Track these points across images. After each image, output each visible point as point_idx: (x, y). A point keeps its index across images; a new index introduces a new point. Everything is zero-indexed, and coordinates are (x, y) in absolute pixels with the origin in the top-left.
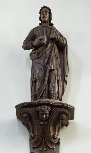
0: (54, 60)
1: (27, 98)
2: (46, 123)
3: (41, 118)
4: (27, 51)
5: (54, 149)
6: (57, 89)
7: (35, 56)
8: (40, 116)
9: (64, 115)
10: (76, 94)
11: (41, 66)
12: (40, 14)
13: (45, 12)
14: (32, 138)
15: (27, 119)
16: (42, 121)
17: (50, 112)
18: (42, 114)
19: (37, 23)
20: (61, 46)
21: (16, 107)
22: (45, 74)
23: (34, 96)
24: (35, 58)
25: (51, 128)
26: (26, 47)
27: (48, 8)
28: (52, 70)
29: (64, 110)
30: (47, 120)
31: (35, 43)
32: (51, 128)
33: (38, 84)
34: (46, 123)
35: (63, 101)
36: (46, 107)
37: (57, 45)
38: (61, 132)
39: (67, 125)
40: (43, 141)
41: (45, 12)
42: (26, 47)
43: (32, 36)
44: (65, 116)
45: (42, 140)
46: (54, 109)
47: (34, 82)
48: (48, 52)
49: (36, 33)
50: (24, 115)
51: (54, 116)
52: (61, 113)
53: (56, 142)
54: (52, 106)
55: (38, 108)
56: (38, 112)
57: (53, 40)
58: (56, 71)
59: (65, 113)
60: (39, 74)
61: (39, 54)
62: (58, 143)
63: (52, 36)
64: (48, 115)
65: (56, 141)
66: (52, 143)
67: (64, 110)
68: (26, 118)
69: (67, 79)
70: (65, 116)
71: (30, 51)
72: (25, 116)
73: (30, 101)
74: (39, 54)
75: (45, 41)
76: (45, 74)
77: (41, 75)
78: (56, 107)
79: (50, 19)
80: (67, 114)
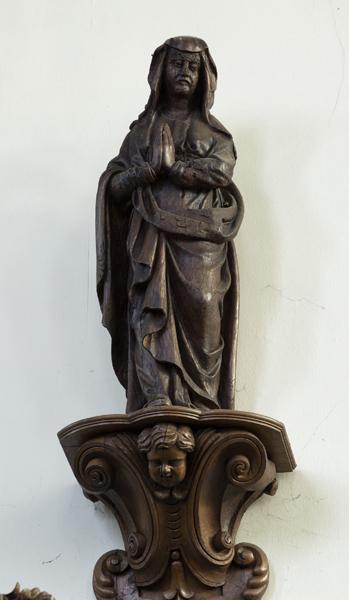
2: (178, 496)
3: (155, 475)
4: (160, 42)
5: (221, 587)
9: (253, 455)
10: (279, 373)
12: (137, 118)
15: (104, 481)
16: (161, 488)
18: (159, 462)
21: (61, 435)
25: (203, 512)
30: (187, 484)
32: (203, 512)
34: (178, 496)
39: (270, 489)
40: (175, 563)
44: (248, 462)
45: (171, 561)
50: (94, 463)
51: (209, 468)
64: (182, 466)
65: (228, 556)
68: (101, 475)
70: (246, 460)
72: (99, 468)
73: (124, 413)
78: (211, 432)
80: (243, 443)
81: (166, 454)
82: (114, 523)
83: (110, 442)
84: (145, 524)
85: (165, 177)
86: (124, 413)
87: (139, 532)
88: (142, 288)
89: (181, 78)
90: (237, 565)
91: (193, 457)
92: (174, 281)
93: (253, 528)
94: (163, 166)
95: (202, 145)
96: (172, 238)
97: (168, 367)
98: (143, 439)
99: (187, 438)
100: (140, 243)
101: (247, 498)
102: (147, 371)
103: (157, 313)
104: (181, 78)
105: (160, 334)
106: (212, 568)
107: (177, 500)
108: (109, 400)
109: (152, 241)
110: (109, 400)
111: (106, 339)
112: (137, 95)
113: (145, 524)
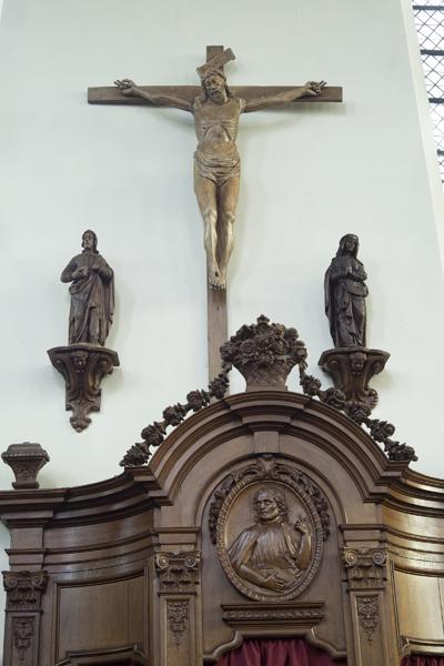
0: (97, 295)
1: (64, 342)
6: (98, 330)
7: (74, 291)
11: (431, 22)
13: (90, 238)
14: (68, 388)
16: (77, 369)
19: (79, 250)
20: (106, 278)
21: (48, 352)
23: (73, 339)
24: (74, 291)
26: (65, 280)
27: (92, 233)
28: (92, 308)
29: (103, 356)
30: (84, 368)
31: (74, 274)
33: (76, 324)
35: (106, 346)
36: (82, 352)
37: (314, 96)
39: (110, 373)
41: (90, 238)
42: (65, 280)
43: (72, 267)
46: (92, 355)
47: (72, 323)
48: (89, 286)
49: (77, 262)
51: (93, 364)
52: (100, 360)
53: (96, 392)
54: (90, 351)
55: (73, 354)
56: (72, 358)
57: (96, 271)
59: (105, 360)
60: (78, 312)
61: (78, 288)
62: (99, 395)
63: (95, 267)
66: (92, 395)
67: (103, 356)
69: (114, 318)
71: (70, 284)
74: (78, 288)
75: (85, 273)
76: (85, 312)
79: (95, 246)
83: (340, 356)
84: (346, 381)
85: (349, 276)
88: (344, 310)
89: (349, 246)
91: (366, 363)
93: (374, 384)
94: (349, 274)
95: (357, 267)
97: (352, 334)
98: (352, 356)
101: (103, 376)
102: (345, 334)
104: (349, 246)
107: (81, 377)
112: (335, 247)
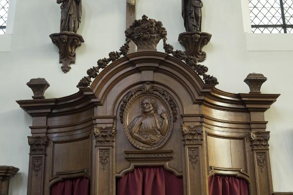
0: (72, 9)
1: (57, 30)
6: (73, 26)
8: (194, 40)
17: (67, 39)
22: (67, 18)
23: (62, 29)
29: (76, 38)
30: (66, 43)
32: (199, 47)
36: (65, 36)
38: (77, 49)
39: (80, 45)
48: (69, 5)
53: (73, 55)
54: (68, 35)
55: (61, 36)
56: (60, 38)
58: (73, 16)
62: (75, 56)
66: (70, 56)
73: (185, 32)
77: (65, 18)
81: (64, 39)
82: (57, 48)
83: (188, 36)
84: (190, 48)
86: (185, 32)
87: (189, 49)
88: (190, 14)
90: (203, 54)
91: (200, 39)
92: (195, 12)
96: (195, 7)
97: (194, 26)
98: (193, 36)
99: (199, 36)
100: (190, 7)
101: (76, 47)
102: (190, 26)
103: (193, 18)
105: (193, 20)
106: (70, 56)
108: (183, 30)
109: (192, 7)
110: (183, 30)
111: (182, 20)
113: (190, 48)
